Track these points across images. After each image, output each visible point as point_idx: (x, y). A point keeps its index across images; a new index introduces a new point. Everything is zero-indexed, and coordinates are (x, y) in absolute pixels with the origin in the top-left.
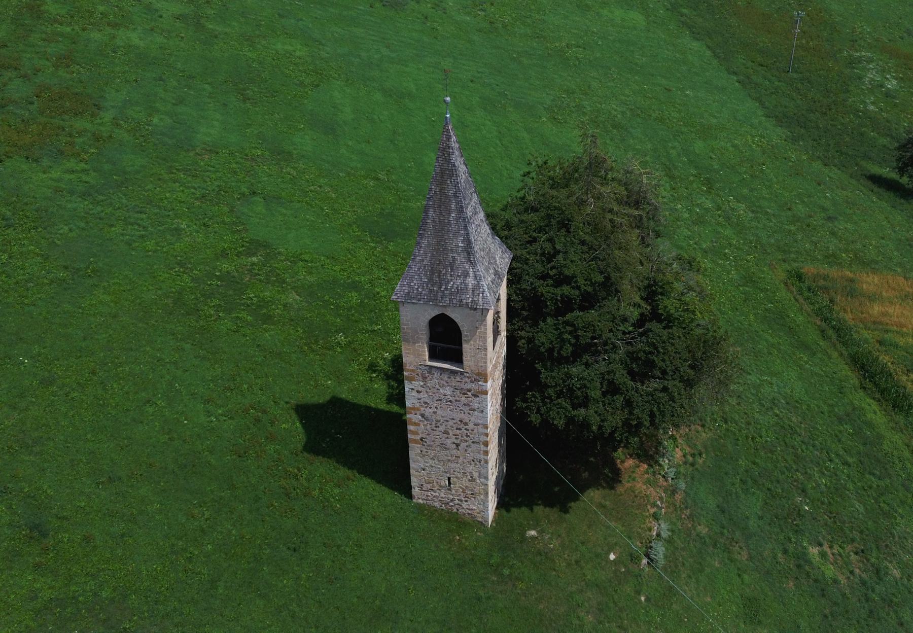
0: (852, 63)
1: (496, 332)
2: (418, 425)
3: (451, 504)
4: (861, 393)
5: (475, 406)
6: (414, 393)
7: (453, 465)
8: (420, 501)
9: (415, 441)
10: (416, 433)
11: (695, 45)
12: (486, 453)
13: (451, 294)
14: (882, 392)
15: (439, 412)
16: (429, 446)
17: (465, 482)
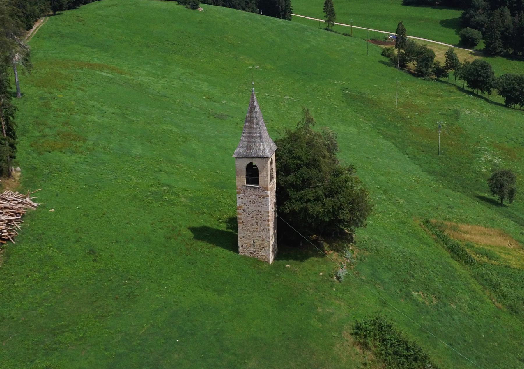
0: (475, 151)
1: (272, 178)
2: (242, 215)
4: (451, 259)
5: (264, 203)
6: (240, 200)
7: (255, 233)
9: (240, 223)
10: (240, 219)
11: (385, 142)
12: (269, 225)
14: (460, 258)
15: (250, 207)
17: (260, 241)
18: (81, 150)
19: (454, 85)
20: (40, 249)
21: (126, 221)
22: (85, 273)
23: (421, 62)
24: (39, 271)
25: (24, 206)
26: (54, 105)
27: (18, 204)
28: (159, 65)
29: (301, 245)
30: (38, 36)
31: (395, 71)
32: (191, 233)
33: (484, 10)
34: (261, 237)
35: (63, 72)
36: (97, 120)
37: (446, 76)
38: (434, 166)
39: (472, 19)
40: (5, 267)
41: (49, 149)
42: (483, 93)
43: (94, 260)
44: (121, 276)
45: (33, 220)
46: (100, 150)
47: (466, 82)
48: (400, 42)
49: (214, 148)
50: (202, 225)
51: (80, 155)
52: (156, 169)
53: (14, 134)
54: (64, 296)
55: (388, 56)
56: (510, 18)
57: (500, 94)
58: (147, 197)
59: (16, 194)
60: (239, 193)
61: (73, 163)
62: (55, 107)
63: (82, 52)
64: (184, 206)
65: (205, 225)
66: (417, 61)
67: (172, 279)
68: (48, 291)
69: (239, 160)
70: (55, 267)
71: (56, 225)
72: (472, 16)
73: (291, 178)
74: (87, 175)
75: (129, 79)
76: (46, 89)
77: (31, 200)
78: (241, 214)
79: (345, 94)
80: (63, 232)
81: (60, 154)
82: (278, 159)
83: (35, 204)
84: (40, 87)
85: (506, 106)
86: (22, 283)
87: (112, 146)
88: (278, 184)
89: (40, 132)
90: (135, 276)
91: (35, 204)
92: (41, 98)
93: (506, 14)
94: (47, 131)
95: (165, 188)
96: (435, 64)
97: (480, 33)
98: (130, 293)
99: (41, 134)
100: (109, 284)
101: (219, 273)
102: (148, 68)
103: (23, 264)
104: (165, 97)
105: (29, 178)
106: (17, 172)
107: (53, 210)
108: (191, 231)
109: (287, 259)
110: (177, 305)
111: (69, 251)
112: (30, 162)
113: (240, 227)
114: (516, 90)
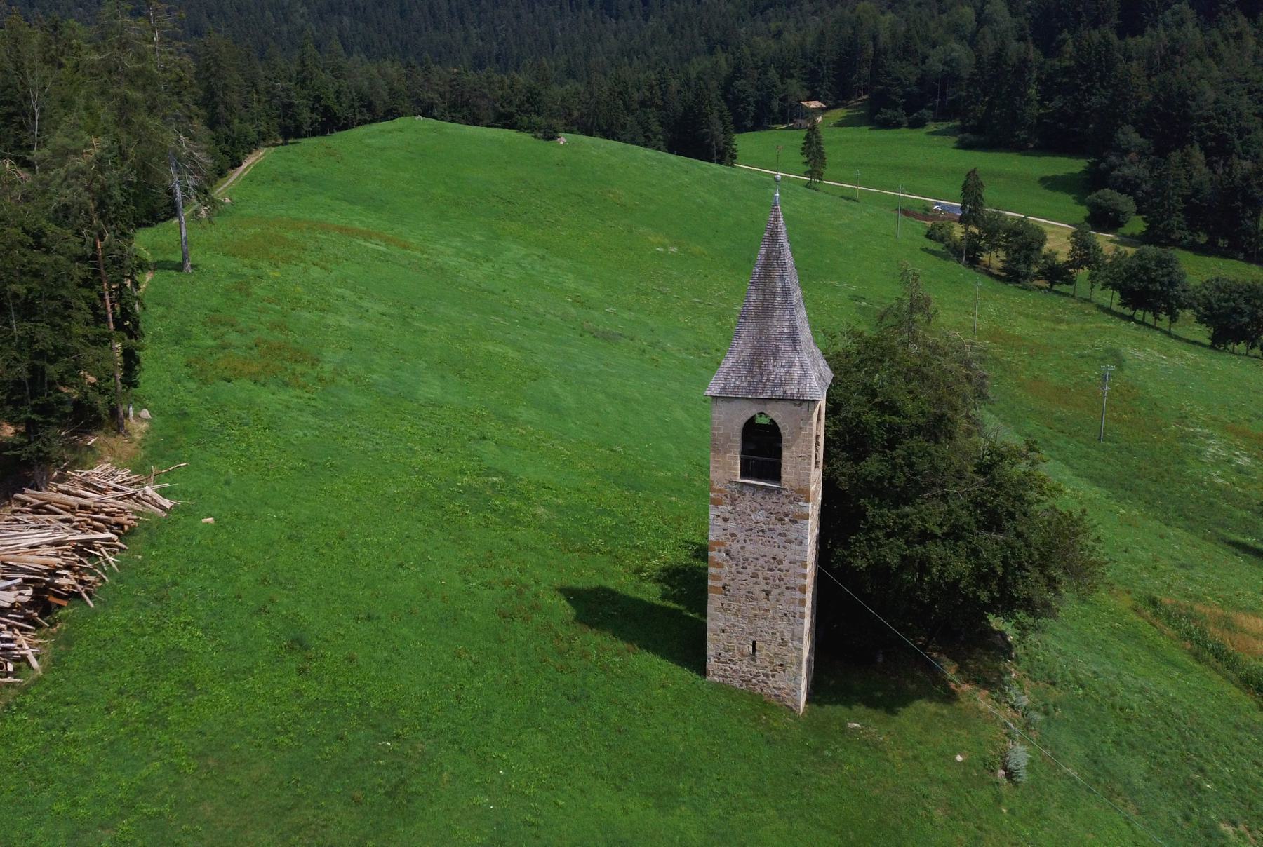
3: (754, 681)
5: (792, 535)
6: (720, 522)
7: (760, 623)
8: (716, 679)
9: (716, 590)
10: (717, 578)
13: (774, 386)
15: (748, 547)
16: (733, 596)
17: (774, 648)
18: (302, 380)
19: (1089, 301)
20: (158, 629)
21: (394, 560)
22: (271, 708)
23: (1016, 251)
24: (142, 695)
25: (136, 507)
26: (257, 290)
27: (122, 499)
28: (479, 238)
29: (880, 660)
30: (250, 179)
31: (959, 269)
32: (568, 605)
33: (1142, 154)
34: (768, 629)
35: (290, 236)
36: (347, 324)
37: (1070, 282)
38: (1098, 464)
39: (1115, 173)
40: (51, 678)
41: (227, 374)
42: (1157, 318)
43: (302, 671)
44: (373, 726)
45: (153, 546)
46: (348, 383)
47: (1117, 294)
48: (972, 210)
49: (601, 396)
50: (594, 585)
51: (298, 392)
52: (474, 434)
53: (136, 326)
54: (202, 781)
55: (941, 240)
56: (1205, 170)
57: (1200, 320)
58: (451, 498)
59: (122, 475)
60: (717, 503)
61: (280, 407)
62: (260, 292)
63: (332, 210)
64: (542, 527)
65: (603, 583)
66: (1006, 248)
67: (517, 746)
68: (158, 764)
69: (723, 406)
70: (190, 685)
71: (211, 563)
72: (1113, 168)
73: (873, 465)
74: (309, 438)
75: (419, 259)
76: (247, 261)
77: (156, 490)
78: (719, 565)
79: (860, 308)
80: (230, 579)
81: (252, 386)
82: (834, 409)
83: (167, 503)
84: (234, 256)
85: (1212, 347)
86: (89, 732)
87: (375, 376)
88: (829, 484)
89: (215, 339)
90: (413, 728)
91: (167, 503)
92: (231, 275)
93: (1194, 160)
94: (233, 337)
95: (495, 479)
96: (1045, 257)
97: (1131, 202)
98: (396, 786)
99: (219, 342)
100: (337, 750)
101: (656, 736)
102: (457, 242)
103: (102, 670)
104: (492, 293)
105: (166, 437)
106: (139, 422)
107: (210, 520)
108: (568, 600)
109: (848, 704)
110: (537, 837)
111: (238, 637)
112: (177, 400)
113: (714, 602)
114: (1242, 313)
